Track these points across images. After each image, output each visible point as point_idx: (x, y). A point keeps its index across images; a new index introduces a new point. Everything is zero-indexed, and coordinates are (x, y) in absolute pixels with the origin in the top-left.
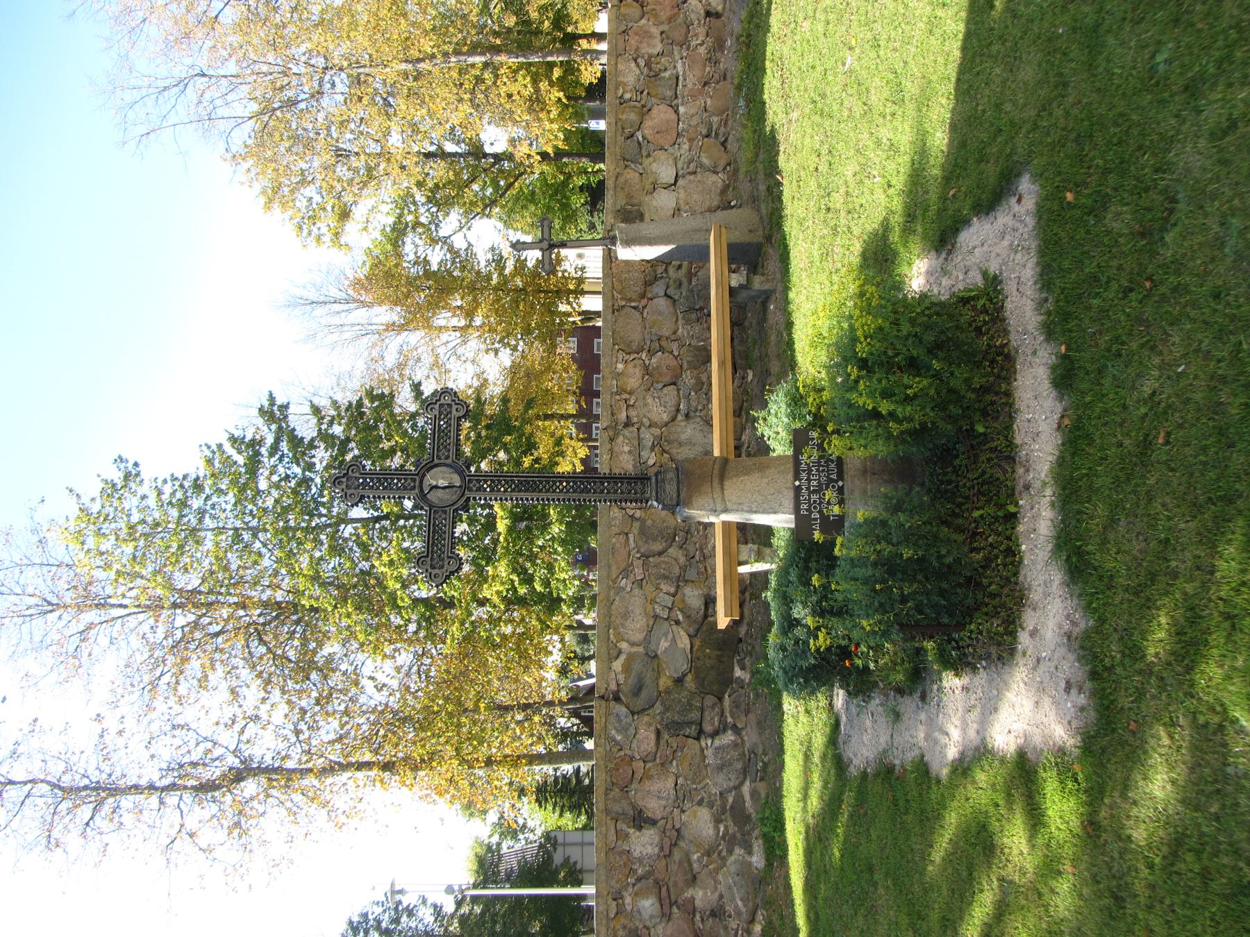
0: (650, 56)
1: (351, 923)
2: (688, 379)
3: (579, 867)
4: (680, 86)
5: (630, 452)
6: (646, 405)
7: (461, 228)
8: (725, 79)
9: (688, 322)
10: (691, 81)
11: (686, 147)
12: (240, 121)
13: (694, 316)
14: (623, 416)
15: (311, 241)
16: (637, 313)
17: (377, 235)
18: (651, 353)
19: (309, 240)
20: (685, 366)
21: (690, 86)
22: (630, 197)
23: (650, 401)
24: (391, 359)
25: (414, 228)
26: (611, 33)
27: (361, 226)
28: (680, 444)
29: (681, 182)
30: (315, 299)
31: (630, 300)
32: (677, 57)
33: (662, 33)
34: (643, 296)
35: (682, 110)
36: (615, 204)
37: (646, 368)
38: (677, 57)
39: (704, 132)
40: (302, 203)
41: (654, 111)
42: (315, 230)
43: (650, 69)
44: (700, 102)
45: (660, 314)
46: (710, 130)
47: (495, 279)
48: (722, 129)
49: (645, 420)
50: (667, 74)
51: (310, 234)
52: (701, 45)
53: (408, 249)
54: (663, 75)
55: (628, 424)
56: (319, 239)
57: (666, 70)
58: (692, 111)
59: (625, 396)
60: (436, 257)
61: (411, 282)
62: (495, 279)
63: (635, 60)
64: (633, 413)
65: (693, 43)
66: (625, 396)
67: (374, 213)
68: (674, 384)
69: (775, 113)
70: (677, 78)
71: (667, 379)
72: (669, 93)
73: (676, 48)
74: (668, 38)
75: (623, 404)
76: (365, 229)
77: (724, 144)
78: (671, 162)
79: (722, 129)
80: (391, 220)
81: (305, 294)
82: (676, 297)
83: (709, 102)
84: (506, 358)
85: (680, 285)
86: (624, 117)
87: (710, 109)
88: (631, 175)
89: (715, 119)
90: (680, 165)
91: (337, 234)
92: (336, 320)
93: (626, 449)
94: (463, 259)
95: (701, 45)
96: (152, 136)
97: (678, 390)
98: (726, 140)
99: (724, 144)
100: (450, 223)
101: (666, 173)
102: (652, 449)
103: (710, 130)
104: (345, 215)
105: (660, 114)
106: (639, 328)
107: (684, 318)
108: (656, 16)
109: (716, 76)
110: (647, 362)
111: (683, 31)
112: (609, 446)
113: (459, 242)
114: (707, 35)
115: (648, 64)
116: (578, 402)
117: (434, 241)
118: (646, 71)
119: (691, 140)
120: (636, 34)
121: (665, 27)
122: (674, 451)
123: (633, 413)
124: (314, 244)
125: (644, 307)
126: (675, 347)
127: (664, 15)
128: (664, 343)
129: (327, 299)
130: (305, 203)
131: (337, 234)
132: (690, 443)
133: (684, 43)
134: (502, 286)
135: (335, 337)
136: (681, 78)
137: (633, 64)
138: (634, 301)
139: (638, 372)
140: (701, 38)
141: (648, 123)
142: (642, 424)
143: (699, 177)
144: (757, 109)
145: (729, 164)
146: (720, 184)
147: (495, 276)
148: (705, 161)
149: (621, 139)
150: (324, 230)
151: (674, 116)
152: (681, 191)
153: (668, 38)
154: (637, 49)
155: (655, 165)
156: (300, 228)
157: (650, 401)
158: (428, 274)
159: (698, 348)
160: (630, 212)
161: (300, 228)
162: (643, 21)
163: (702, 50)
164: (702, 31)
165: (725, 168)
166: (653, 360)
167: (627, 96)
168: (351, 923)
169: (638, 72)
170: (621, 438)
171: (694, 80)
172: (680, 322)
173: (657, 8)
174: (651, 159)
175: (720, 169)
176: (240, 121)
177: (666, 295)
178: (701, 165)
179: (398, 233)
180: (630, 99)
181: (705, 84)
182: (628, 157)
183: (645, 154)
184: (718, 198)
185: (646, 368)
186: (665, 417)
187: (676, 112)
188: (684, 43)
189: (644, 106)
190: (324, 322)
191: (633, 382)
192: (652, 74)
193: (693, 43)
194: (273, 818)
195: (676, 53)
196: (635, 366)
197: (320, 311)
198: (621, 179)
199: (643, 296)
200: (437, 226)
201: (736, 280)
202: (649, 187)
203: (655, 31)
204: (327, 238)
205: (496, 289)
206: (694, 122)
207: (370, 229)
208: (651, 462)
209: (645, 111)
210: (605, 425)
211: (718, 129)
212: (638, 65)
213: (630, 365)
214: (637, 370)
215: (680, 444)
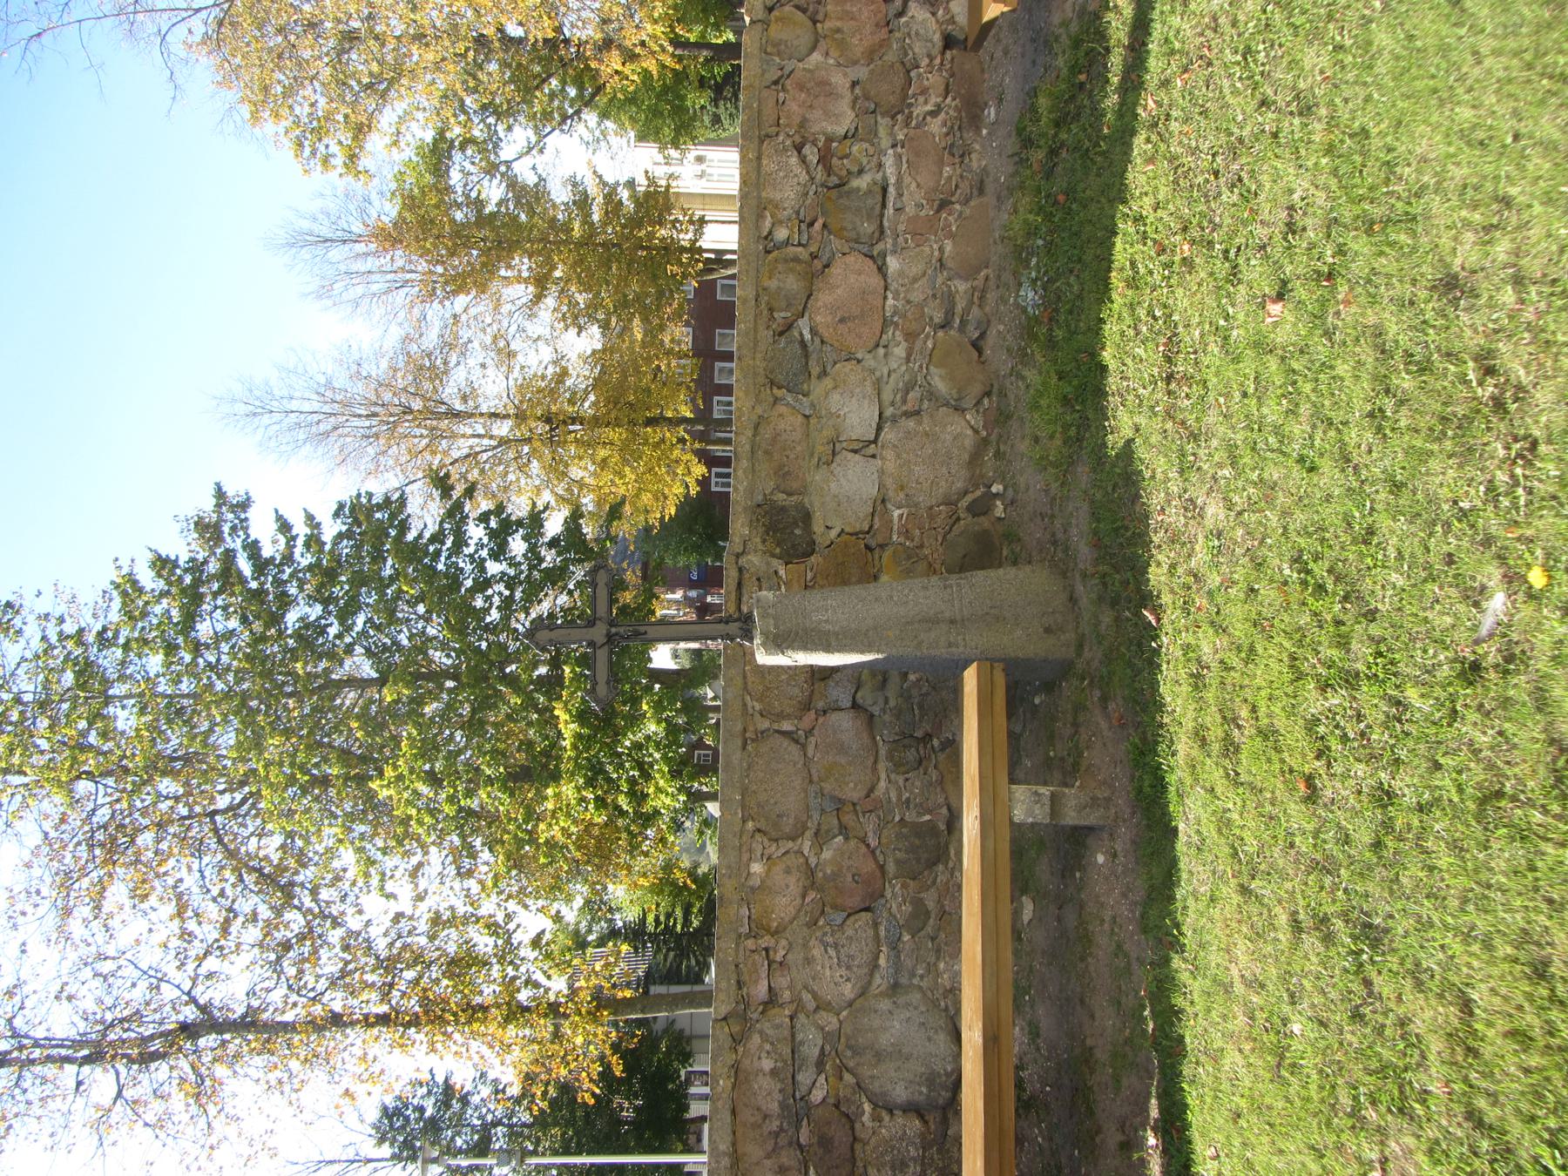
0: (829, 140)
1: (385, 1109)
2: (896, 900)
3: (687, 1032)
4: (890, 211)
5: (774, 1072)
6: (809, 961)
7: (530, 149)
8: (981, 191)
9: (898, 766)
10: (912, 199)
11: (900, 351)
12: (185, 14)
13: (911, 755)
14: (761, 990)
15: (316, 165)
16: (794, 748)
17: (409, 153)
18: (820, 839)
19: (312, 162)
20: (891, 868)
21: (910, 210)
22: (782, 473)
23: (817, 952)
24: (431, 339)
25: (462, 148)
26: (743, 251)
27: (388, 140)
28: (879, 1056)
29: (888, 434)
30: (330, 235)
31: (781, 716)
32: (885, 142)
33: (854, 84)
34: (806, 706)
35: (893, 263)
36: (751, 491)
37: (811, 872)
38: (885, 142)
39: (938, 317)
40: (303, 111)
41: (836, 270)
42: (322, 148)
43: (829, 171)
44: (931, 248)
45: (842, 749)
46: (950, 313)
47: (577, 231)
48: (975, 310)
49: (807, 997)
50: (861, 183)
51: (314, 153)
52: (934, 114)
53: (455, 177)
54: (855, 183)
55: (772, 1000)
56: (326, 161)
57: (861, 172)
58: (915, 270)
59: (766, 941)
60: (494, 192)
61: (459, 231)
62: (577, 231)
63: (799, 148)
64: (781, 981)
65: (919, 110)
66: (766, 941)
67: (402, 129)
68: (867, 909)
69: (1128, 421)
70: (885, 190)
71: (855, 902)
72: (868, 227)
73: (883, 122)
74: (867, 97)
75: (760, 959)
76: (395, 143)
77: (977, 345)
78: (869, 389)
79: (975, 310)
80: (429, 136)
81: (317, 229)
82: (876, 710)
83: (949, 246)
84: (592, 339)
85: (885, 680)
86: (773, 284)
87: (950, 264)
88: (787, 421)
89: (961, 286)
90: (887, 396)
91: (353, 157)
92: (361, 266)
93: (767, 1064)
94: (530, 196)
95: (934, 114)
96: (45, 39)
97: (876, 925)
98: (982, 336)
99: (977, 345)
100: (515, 139)
101: (858, 416)
102: (820, 1065)
103: (950, 313)
104: (361, 131)
105: (849, 276)
106: (797, 783)
107: (890, 757)
108: (842, 45)
109: (965, 186)
110: (813, 861)
111: (899, 81)
112: (730, 1058)
113: (524, 172)
114: (947, 91)
115: (825, 158)
116: (693, 400)
117: (491, 169)
118: (820, 174)
119: (910, 336)
120: (801, 87)
121: (862, 72)
122: (866, 1072)
123: (781, 981)
124: (319, 168)
125: (809, 732)
126: (870, 825)
127: (858, 45)
128: (848, 819)
129: (347, 236)
130: (307, 110)
131: (353, 157)
132: (898, 1054)
133: (899, 109)
134: (587, 241)
135: (360, 290)
136: (891, 190)
137: (794, 160)
138: (788, 717)
139: (794, 884)
140: (935, 99)
141: (823, 298)
142: (799, 1007)
143: (926, 425)
144: (1085, 387)
145: (988, 394)
146: (969, 441)
147: (577, 225)
148: (940, 385)
149: (765, 335)
150: (334, 148)
151: (875, 281)
152: (889, 454)
153: (867, 97)
154: (803, 123)
155: (835, 397)
156: (300, 145)
157: (817, 952)
158: (483, 220)
159: (918, 830)
160: (783, 509)
161: (300, 145)
162: (816, 57)
163: (935, 126)
164: (935, 80)
165: (979, 402)
166: (827, 854)
167: (781, 234)
168: (385, 1109)
169: (804, 177)
170: (756, 1039)
171: (919, 197)
172: (882, 766)
173: (847, 26)
174: (828, 382)
175: (968, 402)
176: (185, 14)
177: (855, 706)
178: (931, 395)
179: (438, 154)
180: (787, 243)
181: (944, 205)
182: (780, 378)
183: (815, 370)
184: (964, 473)
185: (811, 872)
186: (848, 991)
187: (882, 269)
188: (899, 109)
189: (814, 256)
190: (343, 268)
191: (784, 904)
192: (834, 180)
193: (919, 110)
194: (246, 1082)
195: (882, 132)
196: (788, 871)
197: (337, 253)
198: (766, 433)
199: (806, 706)
200: (496, 146)
201: (1026, 805)
202: (822, 449)
203: (840, 80)
204: (338, 161)
205: (580, 244)
206: (916, 296)
207: (402, 144)
208: (817, 1095)
209: (816, 270)
210: (724, 1010)
211: (967, 311)
212: (803, 160)
213: (778, 869)
214: (792, 880)
215: (879, 1056)
